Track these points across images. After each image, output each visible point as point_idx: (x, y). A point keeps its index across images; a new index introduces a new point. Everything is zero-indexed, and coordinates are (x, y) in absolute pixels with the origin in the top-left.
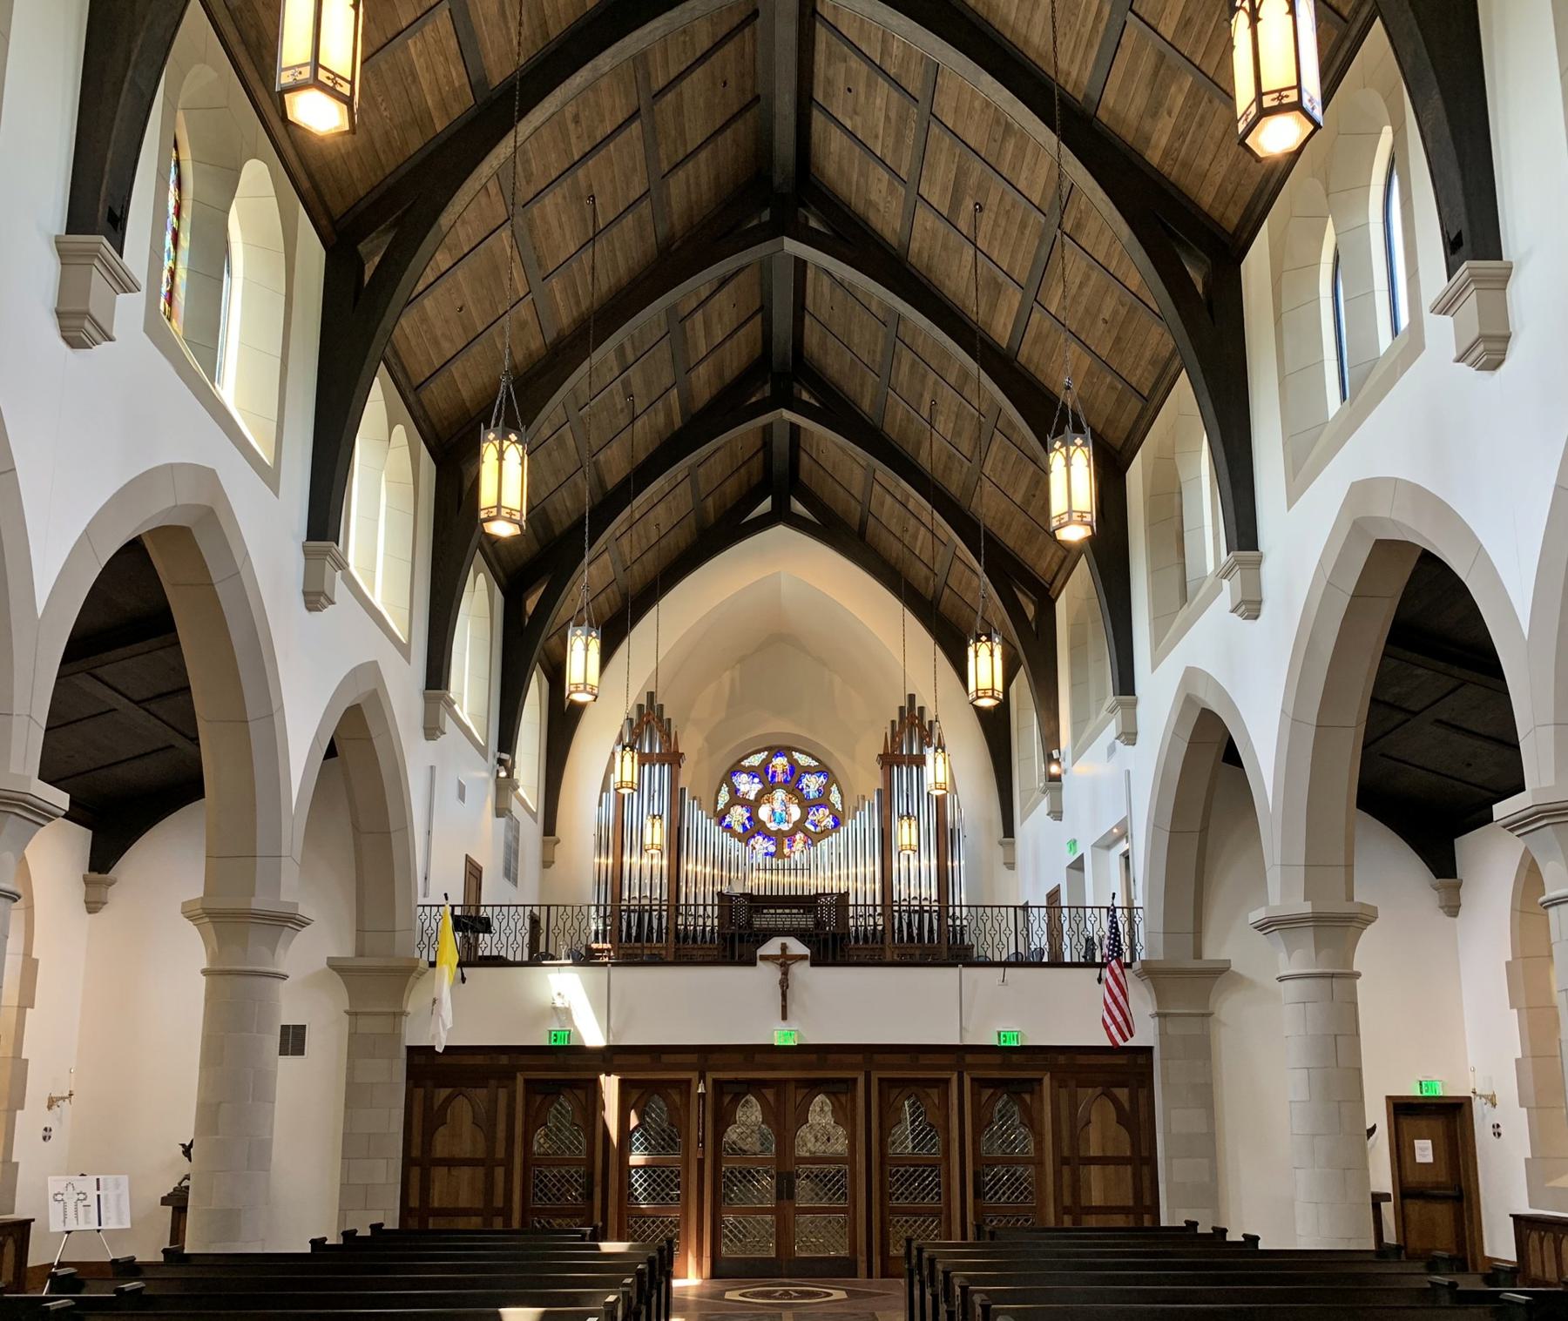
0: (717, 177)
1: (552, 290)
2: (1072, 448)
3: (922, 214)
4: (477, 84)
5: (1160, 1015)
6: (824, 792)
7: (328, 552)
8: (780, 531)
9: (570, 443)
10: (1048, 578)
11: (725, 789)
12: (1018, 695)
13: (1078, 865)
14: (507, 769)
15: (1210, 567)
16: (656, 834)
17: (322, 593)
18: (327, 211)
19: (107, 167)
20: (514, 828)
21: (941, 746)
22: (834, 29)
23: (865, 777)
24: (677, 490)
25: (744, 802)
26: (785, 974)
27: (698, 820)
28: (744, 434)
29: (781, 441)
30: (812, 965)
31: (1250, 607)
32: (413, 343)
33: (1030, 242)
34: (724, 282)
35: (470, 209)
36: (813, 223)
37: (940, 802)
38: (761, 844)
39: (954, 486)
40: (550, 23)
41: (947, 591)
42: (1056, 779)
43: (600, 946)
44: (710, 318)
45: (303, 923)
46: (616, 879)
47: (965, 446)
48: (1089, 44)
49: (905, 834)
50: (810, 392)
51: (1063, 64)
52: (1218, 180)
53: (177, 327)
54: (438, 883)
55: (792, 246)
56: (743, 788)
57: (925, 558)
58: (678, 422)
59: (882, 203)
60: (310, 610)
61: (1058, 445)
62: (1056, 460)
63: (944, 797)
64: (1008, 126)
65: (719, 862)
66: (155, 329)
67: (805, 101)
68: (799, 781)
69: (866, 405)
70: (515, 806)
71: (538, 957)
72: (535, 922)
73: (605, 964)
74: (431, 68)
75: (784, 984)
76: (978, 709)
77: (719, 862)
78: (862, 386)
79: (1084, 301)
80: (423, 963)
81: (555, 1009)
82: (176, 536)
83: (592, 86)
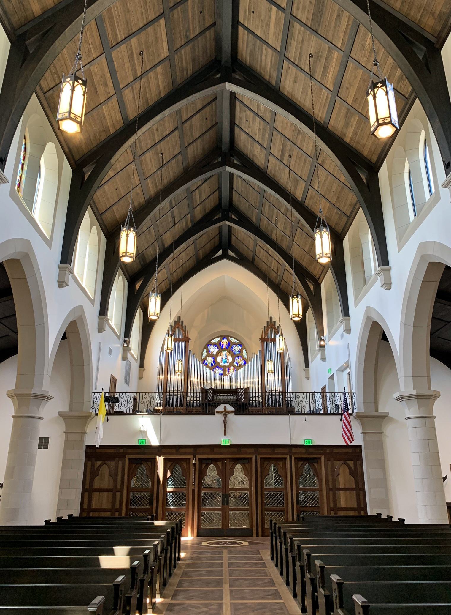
1: (148, 183)
2: (323, 232)
3: (271, 158)
4: (125, 118)
5: (364, 433)
6: (240, 352)
7: (67, 268)
8: (225, 261)
9: (153, 232)
10: (318, 276)
11: (205, 350)
13: (332, 378)
14: (127, 344)
15: (373, 272)
16: (180, 367)
17: (64, 282)
20: (129, 365)
21: (282, 335)
23: (256, 347)
24: (189, 248)
25: (212, 355)
26: (225, 418)
27: (195, 362)
29: (225, 231)
31: (388, 285)
32: (100, 199)
33: (308, 167)
34: (206, 180)
35: (121, 157)
36: (235, 162)
37: (282, 355)
39: (284, 246)
41: (283, 281)
42: (323, 346)
44: (202, 192)
45: (50, 398)
46: (165, 383)
47: (288, 233)
49: (269, 366)
52: (369, 147)
53: (20, 194)
54: (100, 384)
55: (228, 169)
56: (212, 350)
57: (275, 270)
58: (190, 225)
59: (258, 156)
60: (59, 287)
61: (318, 231)
62: (317, 236)
63: (283, 353)
64: (299, 131)
66: (13, 195)
67: (232, 124)
68: (232, 348)
69: (254, 219)
70: (130, 357)
71: (136, 411)
73: (159, 414)
75: (225, 422)
76: (294, 321)
77: (203, 377)
78: (252, 213)
79: (326, 185)
80: (93, 414)
81: (141, 431)
82: (15, 262)
83: (162, 119)
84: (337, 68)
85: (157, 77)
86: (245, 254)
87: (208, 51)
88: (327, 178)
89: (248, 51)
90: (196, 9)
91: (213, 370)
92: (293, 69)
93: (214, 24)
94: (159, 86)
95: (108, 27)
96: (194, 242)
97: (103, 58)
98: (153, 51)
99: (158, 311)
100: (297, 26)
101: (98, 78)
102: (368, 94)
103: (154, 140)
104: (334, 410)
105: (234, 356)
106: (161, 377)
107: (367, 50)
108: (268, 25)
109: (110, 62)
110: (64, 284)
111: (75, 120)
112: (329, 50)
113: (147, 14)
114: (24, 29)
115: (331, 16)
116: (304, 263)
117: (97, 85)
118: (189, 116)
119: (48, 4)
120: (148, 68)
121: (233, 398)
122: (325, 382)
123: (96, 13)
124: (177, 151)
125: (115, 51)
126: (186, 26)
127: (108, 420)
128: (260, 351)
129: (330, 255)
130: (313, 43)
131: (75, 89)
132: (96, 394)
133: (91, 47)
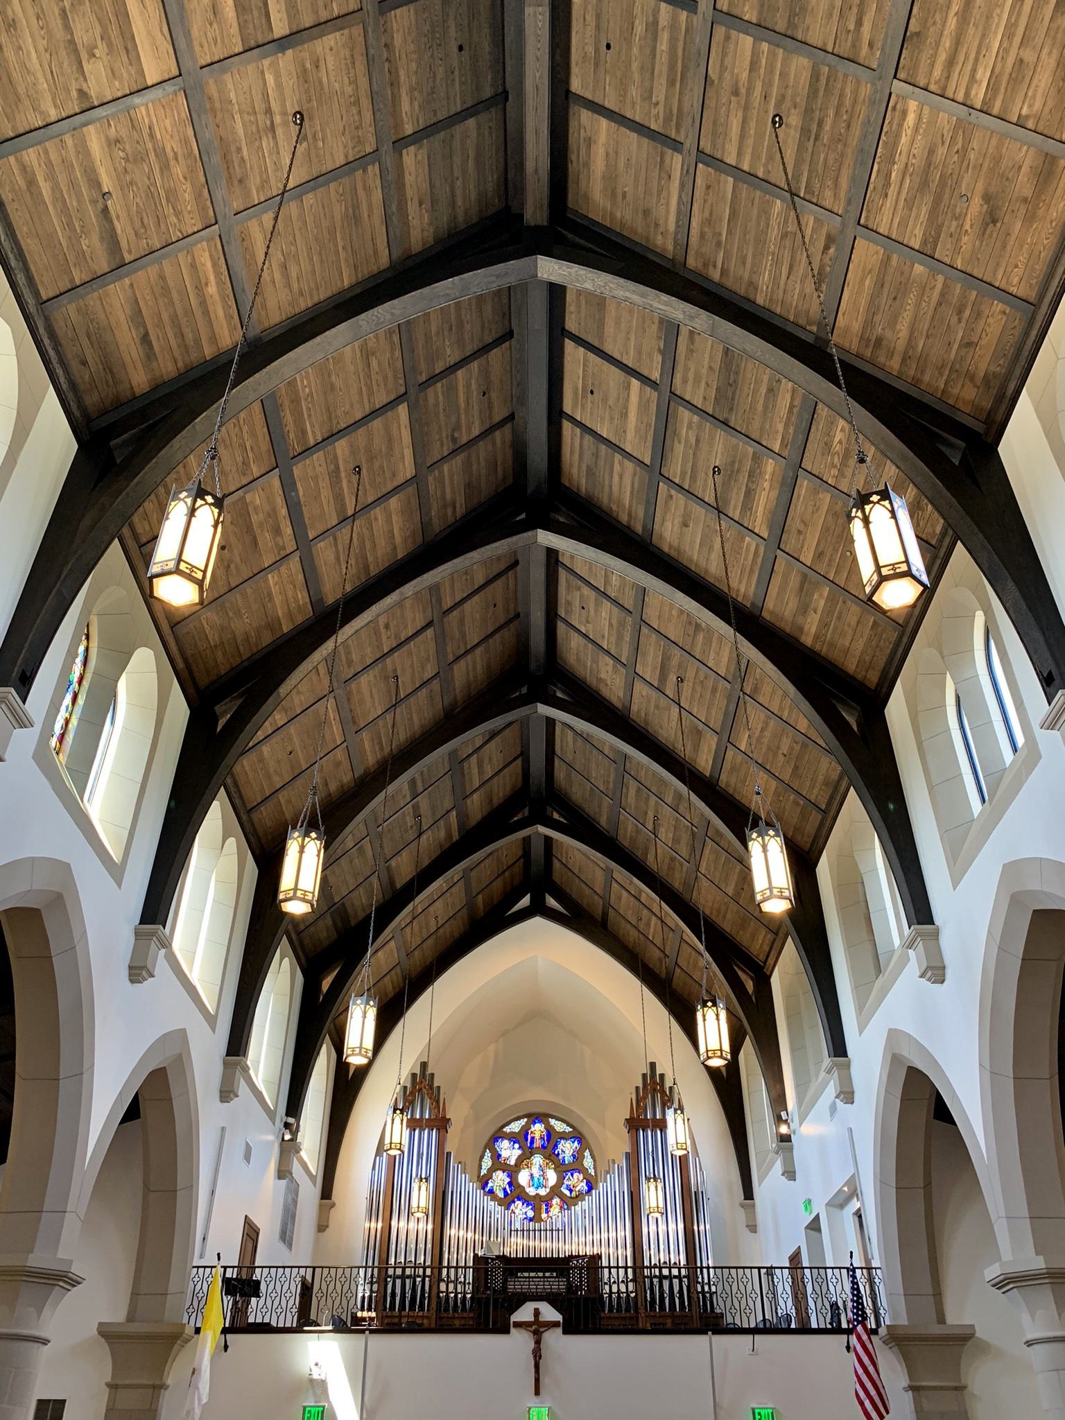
0: (489, 667)
1: (362, 740)
2: (767, 838)
3: (639, 685)
4: (316, 601)
5: (912, 1388)
6: (578, 1157)
7: (154, 934)
8: (537, 922)
9: (369, 852)
10: (762, 957)
11: (488, 1154)
12: (746, 1059)
13: (814, 1226)
14: (291, 1132)
15: (897, 942)
16: (422, 1196)
17: (144, 967)
18: (195, 684)
19: (27, 645)
20: (293, 1190)
21: (681, 1108)
22: (571, 571)
23: (615, 1142)
24: (454, 890)
25: (505, 1167)
26: (538, 1342)
27: (463, 1185)
28: (507, 845)
29: (537, 849)
30: (564, 1333)
31: (936, 972)
32: (251, 777)
33: (720, 702)
34: (493, 735)
35: (304, 683)
36: (559, 694)
37: (683, 1160)
38: (519, 1208)
39: (677, 883)
40: (371, 568)
41: (678, 970)
42: (786, 1139)
43: (365, 1314)
44: (485, 760)
45: (75, 1282)
46: (383, 1244)
47: (684, 851)
48: (752, 571)
49: (652, 1196)
50: (558, 813)
51: (734, 584)
52: (858, 653)
53: (63, 758)
54: (216, 1243)
55: (544, 710)
56: (504, 1154)
57: (658, 942)
58: (456, 837)
59: (610, 681)
60: (132, 981)
61: (754, 835)
62: (755, 847)
63: (686, 1156)
64: (698, 626)
65: (480, 1227)
66: (43, 757)
67: (552, 616)
68: (556, 1146)
69: (603, 821)
70: (296, 1168)
71: (304, 1321)
72: (306, 1290)
73: (363, 1332)
74: (283, 592)
75: (537, 1354)
76: (708, 1068)
77: (480, 1227)
78: (600, 806)
79: (766, 741)
80: (190, 1330)
81: (311, 1381)
83: (400, 604)
84: (774, 494)
85: (389, 520)
86: (584, 903)
87: (500, 469)
88: (767, 724)
89: (584, 468)
90: (474, 386)
91: (508, 1208)
92: (680, 499)
93: (512, 417)
94: (393, 537)
95: (289, 418)
96: (465, 875)
97: (274, 480)
98: (382, 467)
99: (369, 1043)
100: (685, 415)
101: (261, 516)
102: (850, 519)
103: (379, 647)
104: (828, 1320)
105: (563, 1168)
106: (373, 1225)
107: (837, 453)
108: (624, 415)
109: (288, 486)
110: (144, 973)
111: (190, 577)
112: (756, 458)
113: (371, 393)
114: (111, 418)
115: (756, 391)
116: (727, 924)
117: (257, 531)
118: (458, 599)
119: (164, 371)
120: (370, 499)
121: (557, 1285)
122: (799, 1239)
123: (263, 390)
124: (429, 672)
125: (300, 465)
126: (454, 419)
127: (226, 1347)
128: (627, 1154)
129: (789, 893)
130: (719, 447)
131: (197, 513)
132: (201, 1270)
133: (250, 455)
